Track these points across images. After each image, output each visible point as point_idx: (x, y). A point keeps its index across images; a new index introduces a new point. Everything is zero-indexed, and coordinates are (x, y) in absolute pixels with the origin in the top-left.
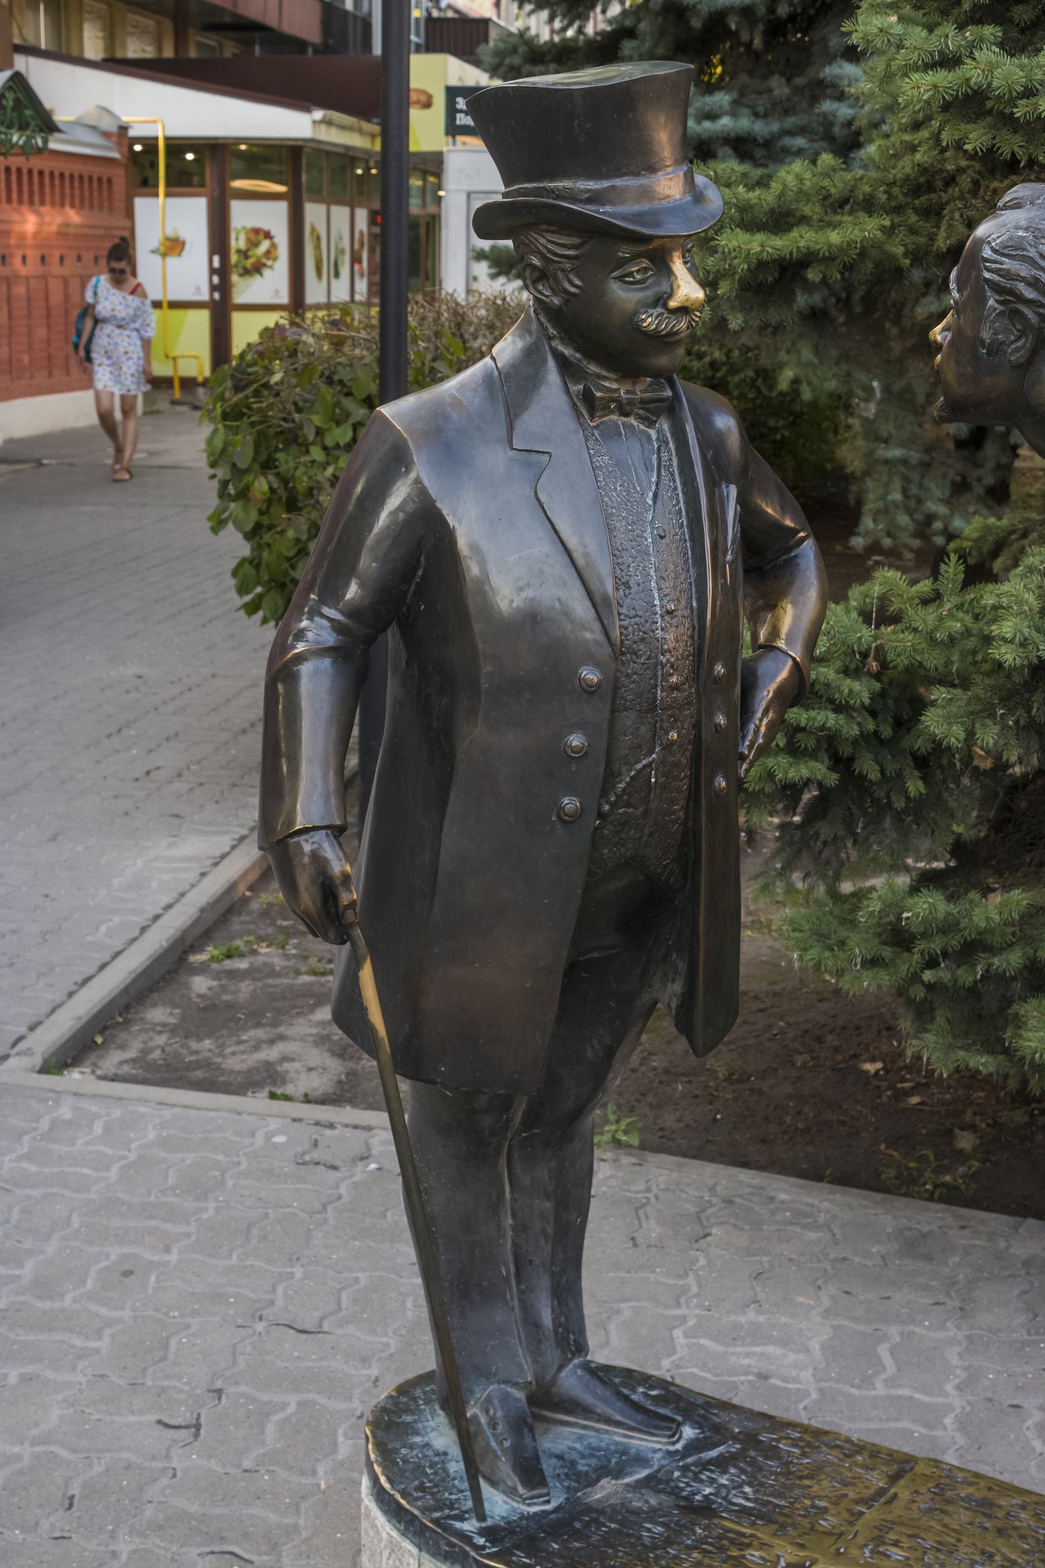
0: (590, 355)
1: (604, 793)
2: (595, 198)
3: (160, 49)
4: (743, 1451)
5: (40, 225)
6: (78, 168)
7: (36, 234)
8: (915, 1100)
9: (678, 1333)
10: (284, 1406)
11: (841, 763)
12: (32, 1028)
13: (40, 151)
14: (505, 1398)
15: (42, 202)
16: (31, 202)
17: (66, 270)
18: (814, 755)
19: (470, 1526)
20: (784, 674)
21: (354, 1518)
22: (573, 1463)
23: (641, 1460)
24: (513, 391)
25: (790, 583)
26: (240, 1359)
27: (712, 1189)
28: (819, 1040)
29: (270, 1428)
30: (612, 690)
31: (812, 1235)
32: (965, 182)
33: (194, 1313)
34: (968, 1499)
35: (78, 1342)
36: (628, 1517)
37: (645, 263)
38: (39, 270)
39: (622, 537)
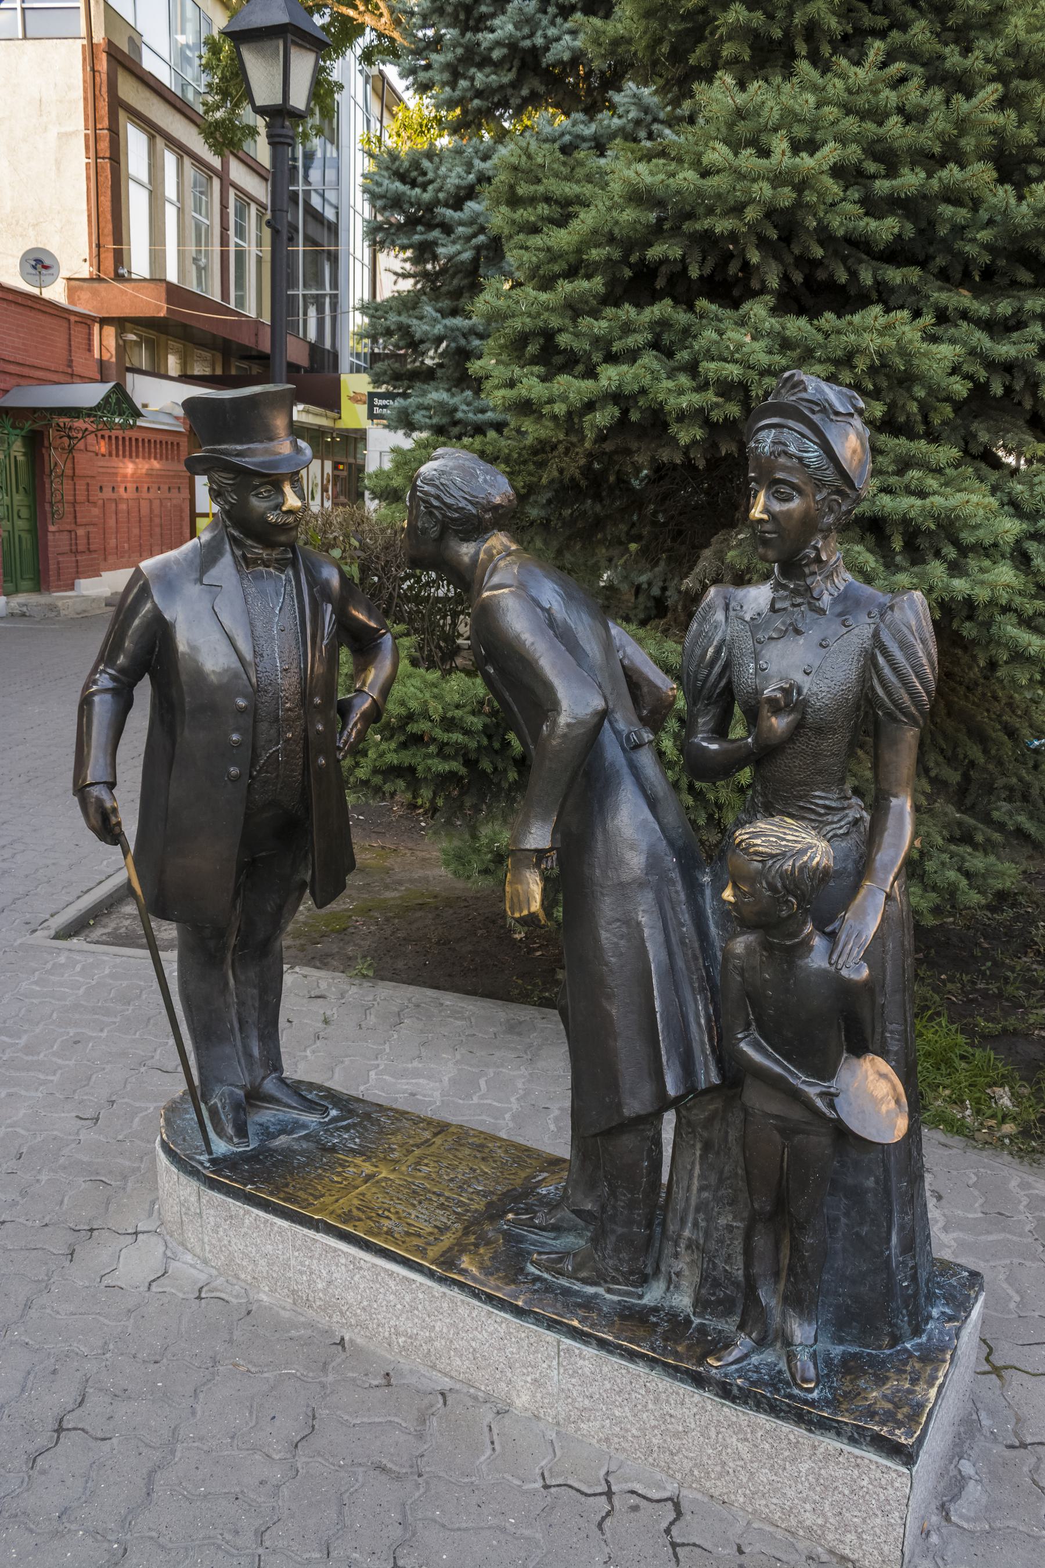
0: (248, 536)
1: (253, 765)
2: (240, 454)
3: (214, 370)
4: (360, 1123)
5: (136, 469)
6: (159, 437)
7: (133, 475)
8: (539, 953)
9: (372, 1074)
10: (147, 1109)
11: (470, 763)
12: (52, 916)
13: (132, 427)
14: (231, 1093)
15: (137, 456)
16: (131, 457)
17: (151, 495)
18: (454, 758)
19: (204, 1158)
20: (366, 705)
21: (154, 1160)
22: (268, 1128)
23: (304, 1126)
24: (208, 557)
25: (375, 657)
26: (129, 1087)
27: (409, 1000)
28: (494, 922)
29: (137, 1120)
30: (253, 712)
31: (459, 1023)
32: (561, 448)
33: (108, 1062)
34: (472, 1144)
35: (42, 1076)
36: (288, 1153)
37: (269, 487)
38: (135, 495)
39: (259, 631)
